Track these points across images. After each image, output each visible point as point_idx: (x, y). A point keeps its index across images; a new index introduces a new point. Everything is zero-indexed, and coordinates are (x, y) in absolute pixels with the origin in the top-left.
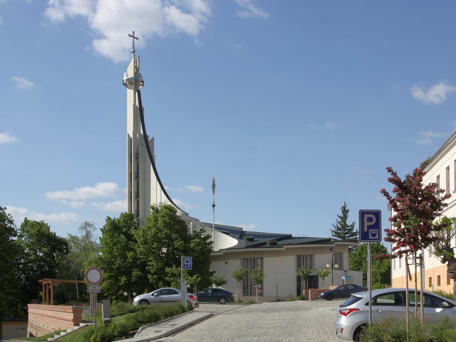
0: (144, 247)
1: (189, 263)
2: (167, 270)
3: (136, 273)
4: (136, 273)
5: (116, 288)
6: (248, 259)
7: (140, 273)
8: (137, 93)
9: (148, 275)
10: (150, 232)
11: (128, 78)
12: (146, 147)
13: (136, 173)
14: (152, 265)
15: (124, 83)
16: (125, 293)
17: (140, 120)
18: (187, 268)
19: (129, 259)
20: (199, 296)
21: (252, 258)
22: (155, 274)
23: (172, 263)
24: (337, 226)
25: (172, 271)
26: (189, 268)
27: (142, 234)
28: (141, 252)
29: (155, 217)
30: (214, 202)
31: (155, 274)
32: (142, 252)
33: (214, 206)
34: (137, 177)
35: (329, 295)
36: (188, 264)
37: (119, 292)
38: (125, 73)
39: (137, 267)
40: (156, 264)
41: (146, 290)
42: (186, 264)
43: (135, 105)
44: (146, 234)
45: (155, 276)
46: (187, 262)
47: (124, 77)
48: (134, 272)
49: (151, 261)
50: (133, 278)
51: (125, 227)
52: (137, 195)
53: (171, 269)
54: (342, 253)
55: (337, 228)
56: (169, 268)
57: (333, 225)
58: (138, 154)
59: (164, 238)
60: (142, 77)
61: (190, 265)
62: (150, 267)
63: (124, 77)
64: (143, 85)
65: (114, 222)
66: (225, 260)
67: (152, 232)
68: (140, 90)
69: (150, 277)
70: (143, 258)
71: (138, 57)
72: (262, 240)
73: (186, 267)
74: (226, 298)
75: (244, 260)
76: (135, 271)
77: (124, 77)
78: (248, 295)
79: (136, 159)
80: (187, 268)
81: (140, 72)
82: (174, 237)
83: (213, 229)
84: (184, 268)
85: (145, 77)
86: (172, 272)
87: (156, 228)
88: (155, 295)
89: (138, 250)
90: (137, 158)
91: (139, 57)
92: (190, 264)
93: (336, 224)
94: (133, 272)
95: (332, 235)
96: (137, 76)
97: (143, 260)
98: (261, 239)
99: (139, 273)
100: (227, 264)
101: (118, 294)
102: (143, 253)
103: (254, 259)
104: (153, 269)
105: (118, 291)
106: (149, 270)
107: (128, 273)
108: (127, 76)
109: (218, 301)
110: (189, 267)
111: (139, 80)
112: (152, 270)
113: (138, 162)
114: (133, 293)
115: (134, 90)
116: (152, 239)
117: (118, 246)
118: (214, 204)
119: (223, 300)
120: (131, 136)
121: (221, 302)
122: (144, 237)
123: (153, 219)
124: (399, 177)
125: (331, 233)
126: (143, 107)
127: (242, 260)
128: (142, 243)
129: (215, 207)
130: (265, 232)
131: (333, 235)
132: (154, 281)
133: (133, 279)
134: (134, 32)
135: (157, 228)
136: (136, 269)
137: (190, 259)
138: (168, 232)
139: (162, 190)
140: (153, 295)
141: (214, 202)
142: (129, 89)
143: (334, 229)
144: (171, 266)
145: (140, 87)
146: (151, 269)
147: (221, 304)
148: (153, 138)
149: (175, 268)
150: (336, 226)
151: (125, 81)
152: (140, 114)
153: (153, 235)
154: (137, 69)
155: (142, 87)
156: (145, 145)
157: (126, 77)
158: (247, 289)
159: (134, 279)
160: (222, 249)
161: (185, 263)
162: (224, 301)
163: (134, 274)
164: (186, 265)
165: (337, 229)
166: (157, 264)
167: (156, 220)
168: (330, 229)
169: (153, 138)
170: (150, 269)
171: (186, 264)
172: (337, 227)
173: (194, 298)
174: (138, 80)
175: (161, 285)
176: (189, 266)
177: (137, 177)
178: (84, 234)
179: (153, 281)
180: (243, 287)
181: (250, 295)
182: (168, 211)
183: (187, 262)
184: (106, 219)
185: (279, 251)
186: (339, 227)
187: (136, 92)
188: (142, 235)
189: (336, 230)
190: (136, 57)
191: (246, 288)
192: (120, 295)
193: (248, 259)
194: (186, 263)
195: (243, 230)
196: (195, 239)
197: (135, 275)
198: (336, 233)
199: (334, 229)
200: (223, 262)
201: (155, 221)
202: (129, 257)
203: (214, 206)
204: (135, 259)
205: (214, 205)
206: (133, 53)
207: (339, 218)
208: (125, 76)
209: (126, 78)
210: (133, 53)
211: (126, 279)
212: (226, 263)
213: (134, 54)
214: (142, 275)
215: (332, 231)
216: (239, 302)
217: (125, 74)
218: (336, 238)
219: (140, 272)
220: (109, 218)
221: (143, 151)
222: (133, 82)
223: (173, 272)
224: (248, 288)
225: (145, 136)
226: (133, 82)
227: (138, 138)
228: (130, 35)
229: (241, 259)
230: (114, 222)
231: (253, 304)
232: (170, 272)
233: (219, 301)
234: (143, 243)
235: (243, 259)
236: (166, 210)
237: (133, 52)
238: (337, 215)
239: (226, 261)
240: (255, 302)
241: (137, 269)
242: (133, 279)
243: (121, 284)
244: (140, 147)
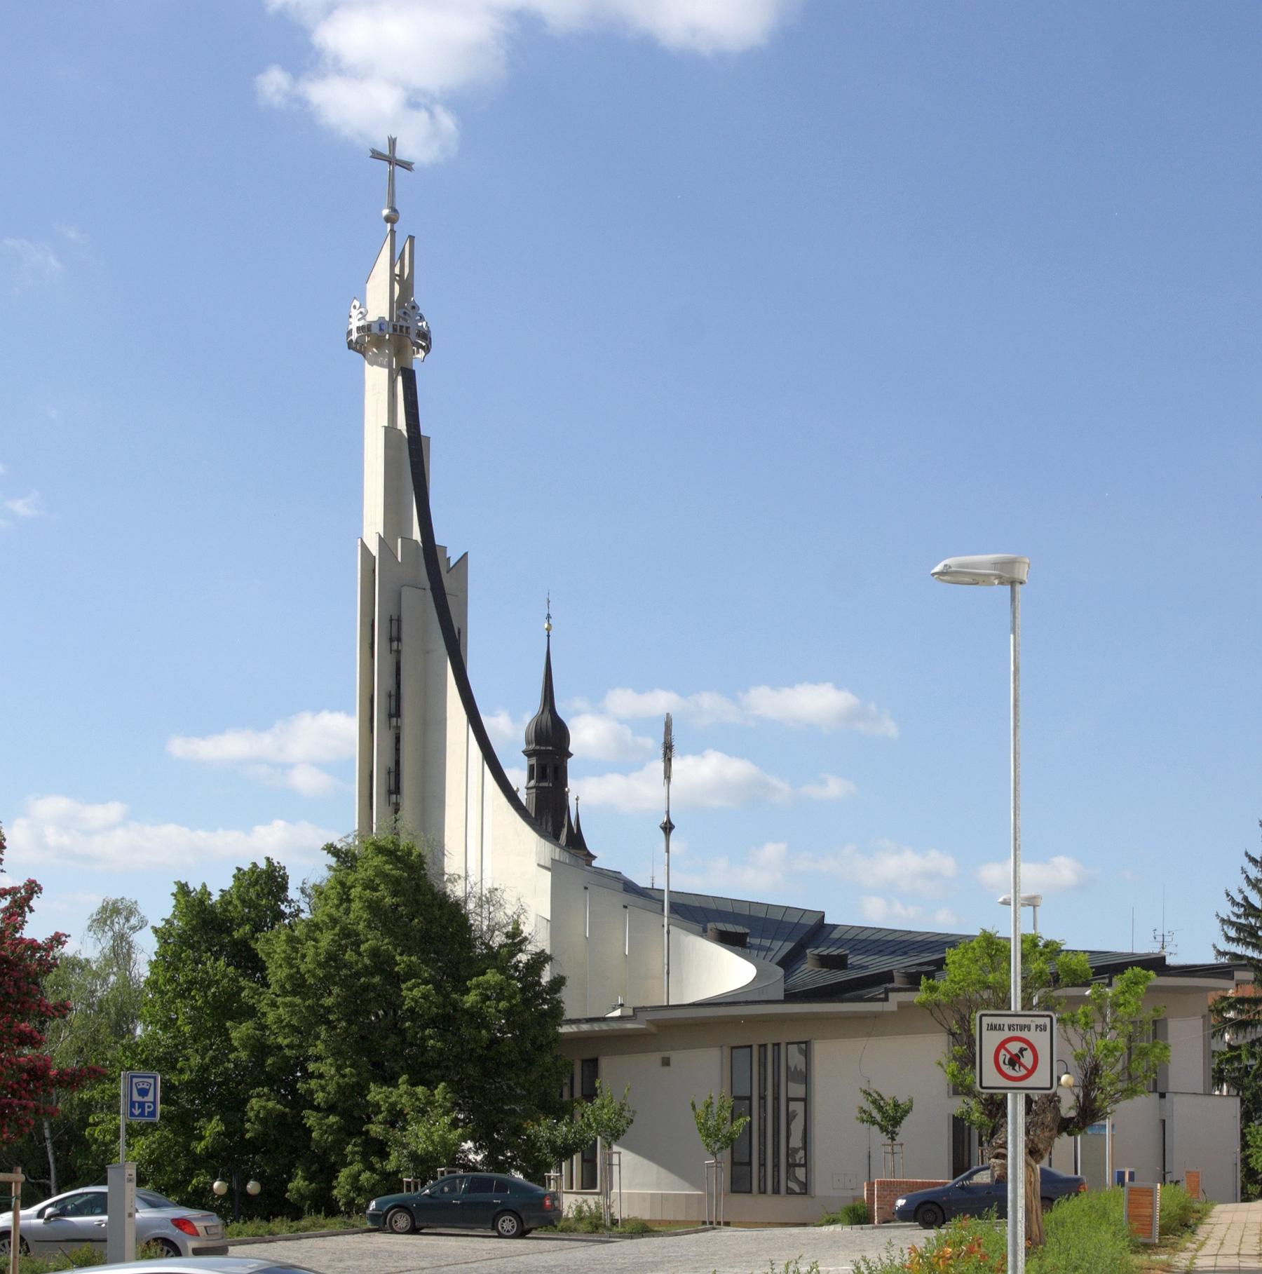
0: (292, 1005)
1: (150, 1097)
2: (376, 1093)
3: (259, 1104)
4: (259, 1104)
5: (182, 1163)
6: (750, 1047)
7: (279, 1107)
8: (400, 379)
9: (306, 1112)
10: (314, 946)
11: (366, 324)
12: (429, 594)
13: (390, 696)
14: (321, 1076)
15: (351, 340)
16: (216, 1184)
17: (413, 488)
18: (142, 1114)
19: (239, 1052)
20: (417, 1205)
21: (770, 1041)
22: (331, 1109)
23: (397, 1069)
24: (1246, 899)
25: (390, 1100)
26: (148, 1116)
27: (285, 952)
28: (282, 1021)
29: (342, 884)
30: (668, 812)
31: (331, 1109)
32: (284, 1024)
33: (668, 828)
34: (395, 712)
35: (929, 1206)
36: (146, 1099)
37: (194, 1181)
38: (356, 303)
39: (270, 1081)
40: (333, 1071)
41: (300, 1173)
42: (140, 1099)
43: (390, 431)
44: (299, 955)
45: (331, 1117)
46: (143, 1092)
47: (350, 317)
48: (254, 1101)
49: (318, 1058)
50: (248, 1125)
51: (245, 920)
52: (393, 782)
53: (391, 1093)
54: (1165, 1020)
55: (1242, 909)
56: (385, 1088)
57: (1228, 895)
58: (399, 620)
59: (367, 971)
60: (422, 318)
61: (154, 1103)
62: (313, 1083)
63: (351, 320)
64: (427, 349)
65: (202, 902)
66: (658, 1050)
67: (322, 944)
68: (414, 368)
69: (311, 1118)
70: (290, 1046)
71: (410, 236)
72: (878, 964)
73: (137, 1112)
74: (523, 1217)
75: (734, 1051)
76: (259, 1096)
77: (350, 317)
78: (750, 1192)
79: (391, 640)
80: (142, 1114)
81: (418, 297)
82: (402, 966)
83: (666, 919)
84: (132, 1114)
85: (432, 316)
86: (390, 1104)
87: (337, 930)
88: (45, 1217)
89: (271, 1017)
90: (394, 637)
91: (412, 238)
92: (152, 1100)
93: (1241, 891)
94: (246, 1100)
95: (1223, 938)
96: (403, 316)
97: (287, 1052)
98: (877, 961)
99: (271, 1104)
100: (666, 1068)
101: (189, 1189)
102: (289, 1025)
103: (774, 1045)
104: (323, 1088)
105: (189, 1173)
106: (311, 1092)
107: (233, 1106)
108: (361, 313)
109: (490, 1226)
110: (148, 1112)
111: (408, 328)
112: (321, 1094)
113: (398, 652)
114: (249, 1186)
115: (390, 366)
116: (320, 973)
117: (194, 998)
118: (669, 821)
119: (507, 1224)
120: (374, 550)
121: (500, 1228)
122: (291, 966)
123: (333, 894)
124: (38, 883)
125: (1223, 930)
126: (423, 433)
127: (727, 1051)
128: (285, 988)
129: (673, 832)
130: (912, 930)
131: (1229, 939)
132: (329, 1140)
133: (251, 1130)
134: (392, 142)
135: (342, 929)
136: (263, 1087)
137: (151, 1081)
138: (386, 944)
139: (487, 763)
140: (40, 1214)
141: (668, 812)
142: (372, 364)
143: (1227, 910)
144: (390, 1080)
145: (418, 356)
146: (317, 1091)
147: (500, 1236)
148: (466, 554)
149: (403, 1088)
150: (1239, 899)
151: (355, 336)
152: (411, 461)
153: (322, 958)
154: (403, 284)
155: (426, 354)
156: (427, 585)
157: (359, 320)
158: (746, 1168)
159: (256, 1130)
160: (644, 1007)
161: (136, 1097)
162: (513, 1227)
163: (252, 1109)
164: (137, 1105)
165: (1245, 910)
166: (339, 1069)
167: (345, 899)
168: (1217, 915)
169: (466, 554)
170: (313, 1090)
171: (140, 1099)
172: (1242, 902)
173: (194, 1228)
174: (404, 330)
175: (354, 1153)
176: (149, 1107)
177: (395, 712)
178: (107, 942)
179: (326, 1136)
180: (732, 1158)
181: (760, 1192)
182: (386, 862)
183: (143, 1092)
184: (173, 894)
185: (877, 1016)
186: (1252, 906)
187: (396, 377)
188: (283, 955)
189: (1238, 916)
190: (401, 240)
191: (741, 1164)
192: (196, 1190)
193: (750, 1047)
194: (139, 1095)
195: (827, 921)
196: (484, 974)
197: (259, 1112)
198: (1239, 928)
199: (1227, 910)
200: (656, 1058)
201: (341, 901)
202: (236, 1044)
203: (668, 828)
204: (261, 1049)
205: (668, 826)
206: (389, 225)
207: (1253, 867)
208: (354, 313)
209: (361, 323)
210: (389, 225)
211: (221, 1128)
212: (666, 1062)
213: (395, 225)
214: (284, 1115)
215: (1223, 921)
216: (590, 1229)
217: (355, 307)
218: (1240, 949)
219: (278, 1102)
220: (183, 889)
221: (420, 606)
222: (387, 337)
223: (393, 1105)
224: (750, 1164)
225: (430, 549)
226: (387, 337)
227: (399, 560)
228: (376, 155)
229: (721, 1047)
230: (202, 902)
231: (643, 1237)
232: (385, 1102)
233: (494, 1227)
234: (287, 986)
235: (732, 1048)
236: (378, 860)
237: (388, 219)
238: (1247, 854)
239: (666, 1054)
240: (654, 1231)
241: (266, 1090)
242: (251, 1130)
243: (199, 1149)
244: (407, 593)
